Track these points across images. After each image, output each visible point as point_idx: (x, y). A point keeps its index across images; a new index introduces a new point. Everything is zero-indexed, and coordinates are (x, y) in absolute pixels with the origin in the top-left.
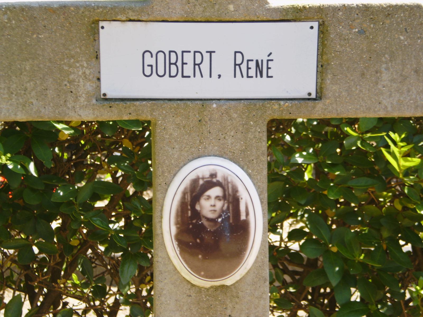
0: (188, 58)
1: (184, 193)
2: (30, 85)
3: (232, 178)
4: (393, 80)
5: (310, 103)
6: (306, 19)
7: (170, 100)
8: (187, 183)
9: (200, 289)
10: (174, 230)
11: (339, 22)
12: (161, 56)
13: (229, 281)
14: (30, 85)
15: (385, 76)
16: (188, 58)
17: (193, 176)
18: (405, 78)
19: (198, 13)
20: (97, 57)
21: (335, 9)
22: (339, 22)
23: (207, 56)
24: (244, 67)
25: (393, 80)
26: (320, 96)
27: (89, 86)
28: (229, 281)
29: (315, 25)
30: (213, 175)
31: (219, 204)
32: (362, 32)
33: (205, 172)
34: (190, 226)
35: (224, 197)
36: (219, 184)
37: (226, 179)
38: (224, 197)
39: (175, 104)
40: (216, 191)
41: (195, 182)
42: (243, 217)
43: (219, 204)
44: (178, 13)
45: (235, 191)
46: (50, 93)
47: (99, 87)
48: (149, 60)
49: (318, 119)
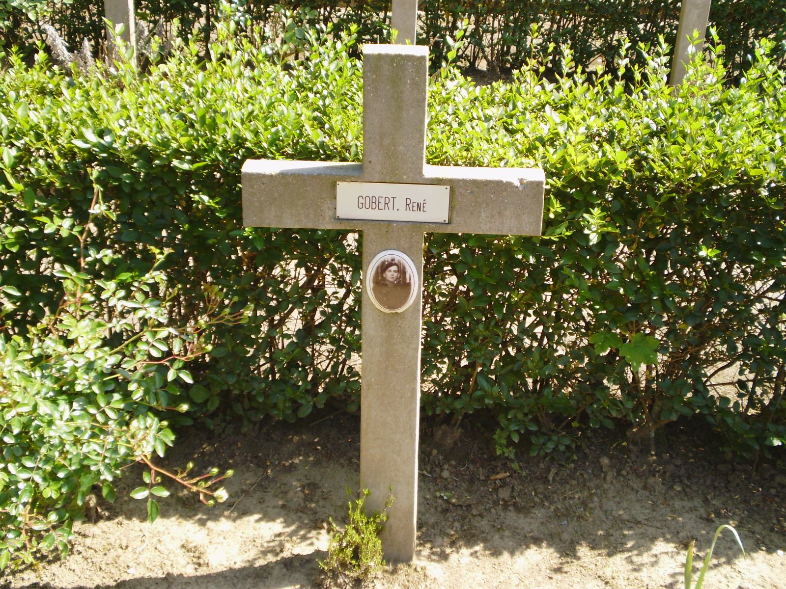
0: (382, 200)
1: (378, 268)
2: (301, 212)
3: (403, 261)
4: (487, 217)
5: (445, 226)
6: (444, 184)
7: (347, 219)
8: (379, 263)
9: (385, 314)
10: (372, 285)
11: (461, 187)
12: (368, 199)
13: (400, 310)
14: (301, 212)
15: (483, 215)
16: (382, 200)
17: (382, 260)
18: (493, 216)
19: (388, 178)
20: (335, 198)
21: (458, 181)
22: (461, 187)
23: (391, 200)
24: (411, 206)
25: (487, 217)
26: (449, 223)
27: (331, 213)
28: (400, 310)
29: (449, 187)
30: (393, 260)
31: (396, 274)
32: (472, 192)
33: (389, 258)
34: (184, 402)
35: (398, 271)
36: (395, 264)
37: (399, 262)
38: (398, 271)
39: (374, 223)
40: (394, 268)
41: (383, 263)
42: (408, 281)
43: (396, 274)
44: (377, 177)
45: (404, 268)
46: (311, 216)
47: (335, 213)
48: (361, 200)
49: (361, 254)
